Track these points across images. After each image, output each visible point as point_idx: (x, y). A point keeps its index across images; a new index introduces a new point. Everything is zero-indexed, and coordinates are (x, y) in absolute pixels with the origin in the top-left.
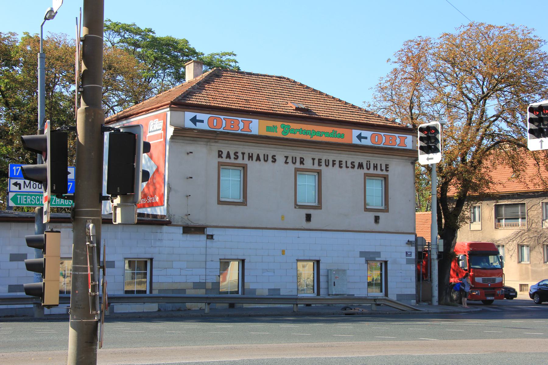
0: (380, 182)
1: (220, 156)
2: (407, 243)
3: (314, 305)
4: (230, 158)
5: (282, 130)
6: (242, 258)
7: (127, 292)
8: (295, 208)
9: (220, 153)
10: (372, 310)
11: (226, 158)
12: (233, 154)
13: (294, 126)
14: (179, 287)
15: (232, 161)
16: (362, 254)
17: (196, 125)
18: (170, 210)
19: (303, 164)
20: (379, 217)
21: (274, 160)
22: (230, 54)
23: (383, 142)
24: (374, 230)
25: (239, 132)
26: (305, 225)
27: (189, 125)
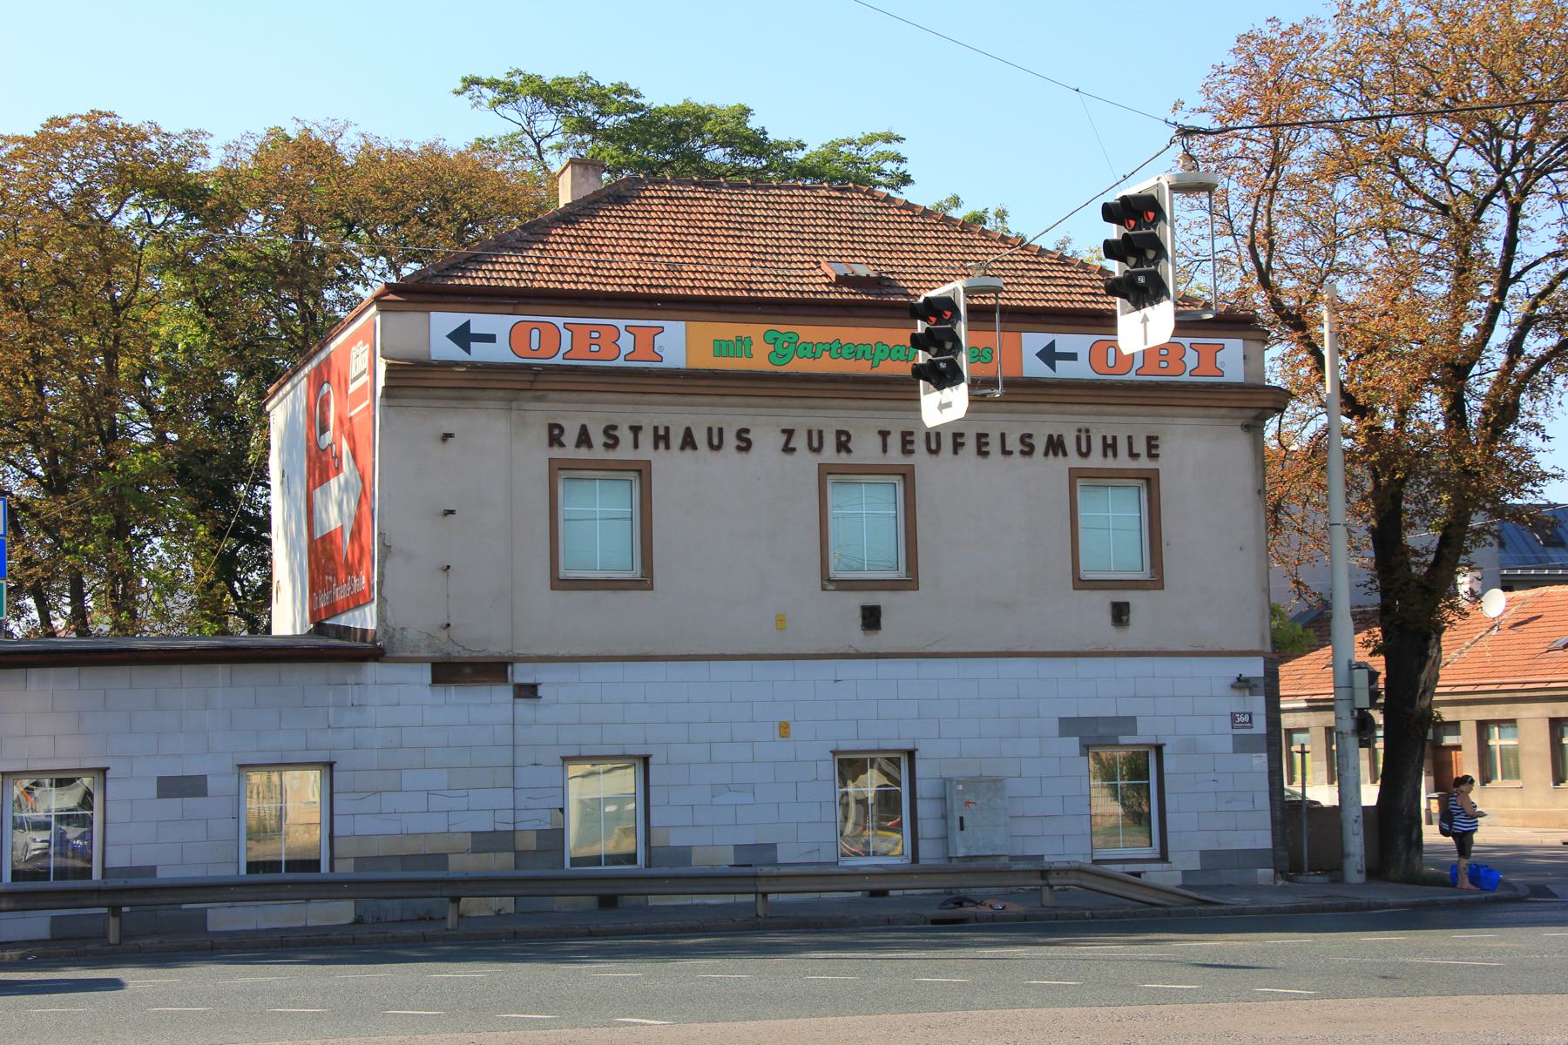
0: (1134, 493)
1: (555, 438)
2: (1233, 686)
3: (900, 893)
4: (590, 446)
5: (771, 348)
6: (642, 751)
7: (253, 867)
8: (824, 588)
9: (843, 438)
10: (1042, 906)
11: (578, 445)
12: (601, 431)
13: (811, 333)
14: (427, 849)
15: (598, 453)
16: (1068, 726)
17: (1053, 368)
18: (389, 614)
19: (849, 451)
20: (1127, 604)
21: (744, 445)
22: (888, 138)
23: (563, 350)
24: (1110, 649)
25: (1185, 378)
26: (858, 638)
27: (445, 350)
